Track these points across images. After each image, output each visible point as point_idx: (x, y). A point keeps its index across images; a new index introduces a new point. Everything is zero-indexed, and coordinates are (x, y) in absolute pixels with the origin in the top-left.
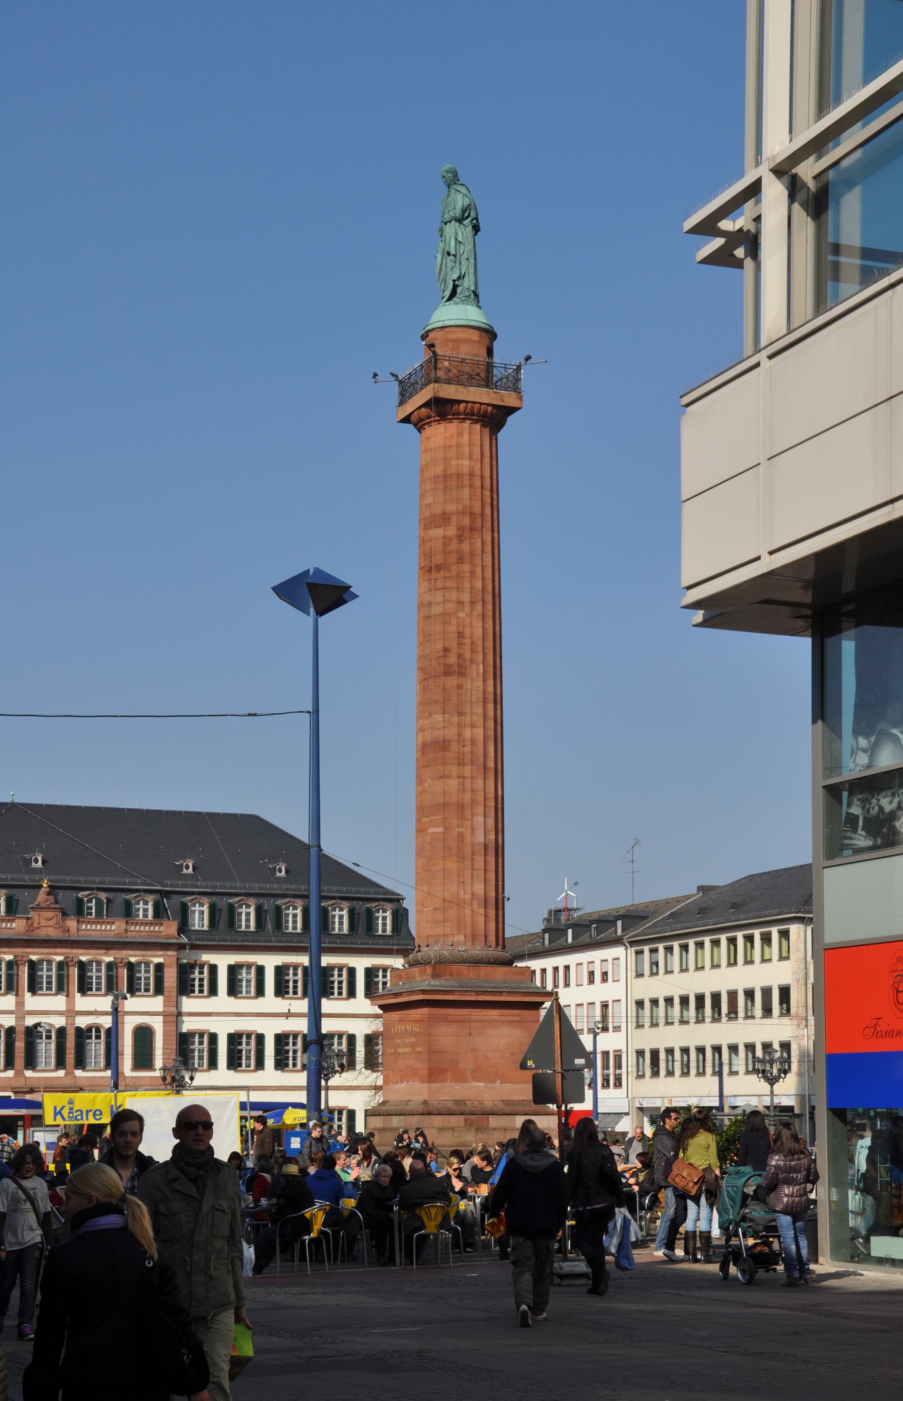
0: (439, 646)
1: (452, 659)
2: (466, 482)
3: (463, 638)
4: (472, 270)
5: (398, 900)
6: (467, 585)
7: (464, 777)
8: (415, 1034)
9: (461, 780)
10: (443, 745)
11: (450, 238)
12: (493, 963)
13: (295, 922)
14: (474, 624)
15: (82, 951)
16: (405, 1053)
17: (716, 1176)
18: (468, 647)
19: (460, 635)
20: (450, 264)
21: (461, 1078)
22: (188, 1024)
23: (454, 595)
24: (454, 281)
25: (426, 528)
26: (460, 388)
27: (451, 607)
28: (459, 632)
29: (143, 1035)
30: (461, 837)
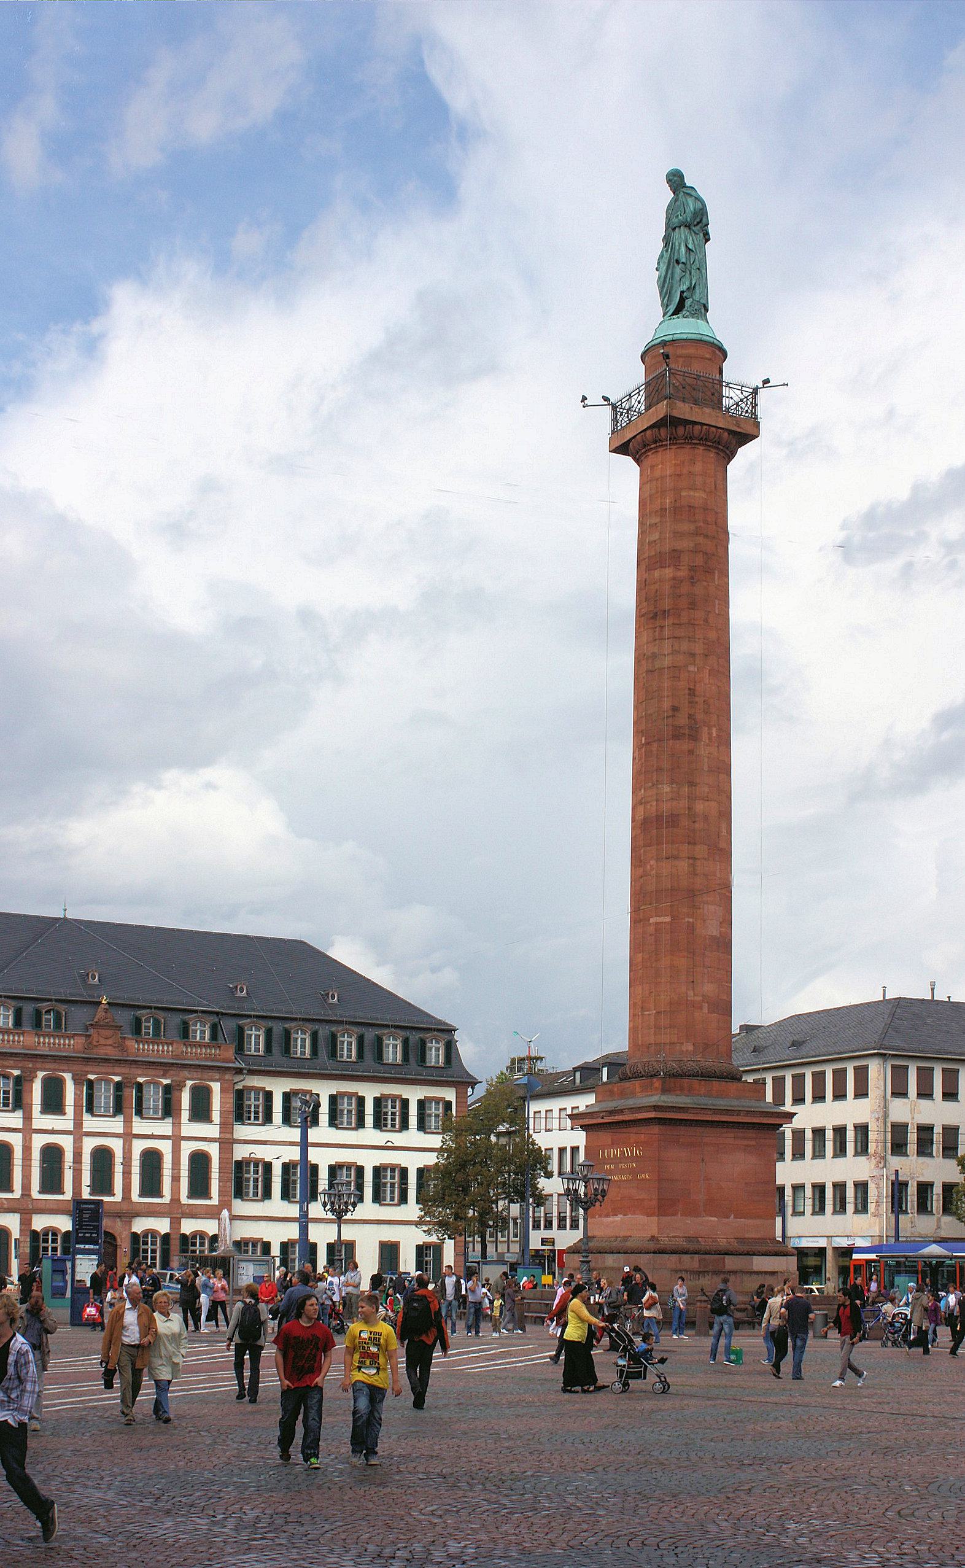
0: (666, 704)
1: (682, 720)
5: (451, 1031)
7: (695, 859)
8: (636, 1159)
9: (691, 861)
10: (673, 820)
11: (680, 245)
12: (726, 1077)
13: (349, 1050)
15: (140, 1072)
16: (621, 1181)
17: (681, 1310)
21: (692, 1211)
22: (241, 1152)
23: (685, 646)
24: (682, 292)
25: (649, 569)
26: (696, 409)
30: (691, 928)
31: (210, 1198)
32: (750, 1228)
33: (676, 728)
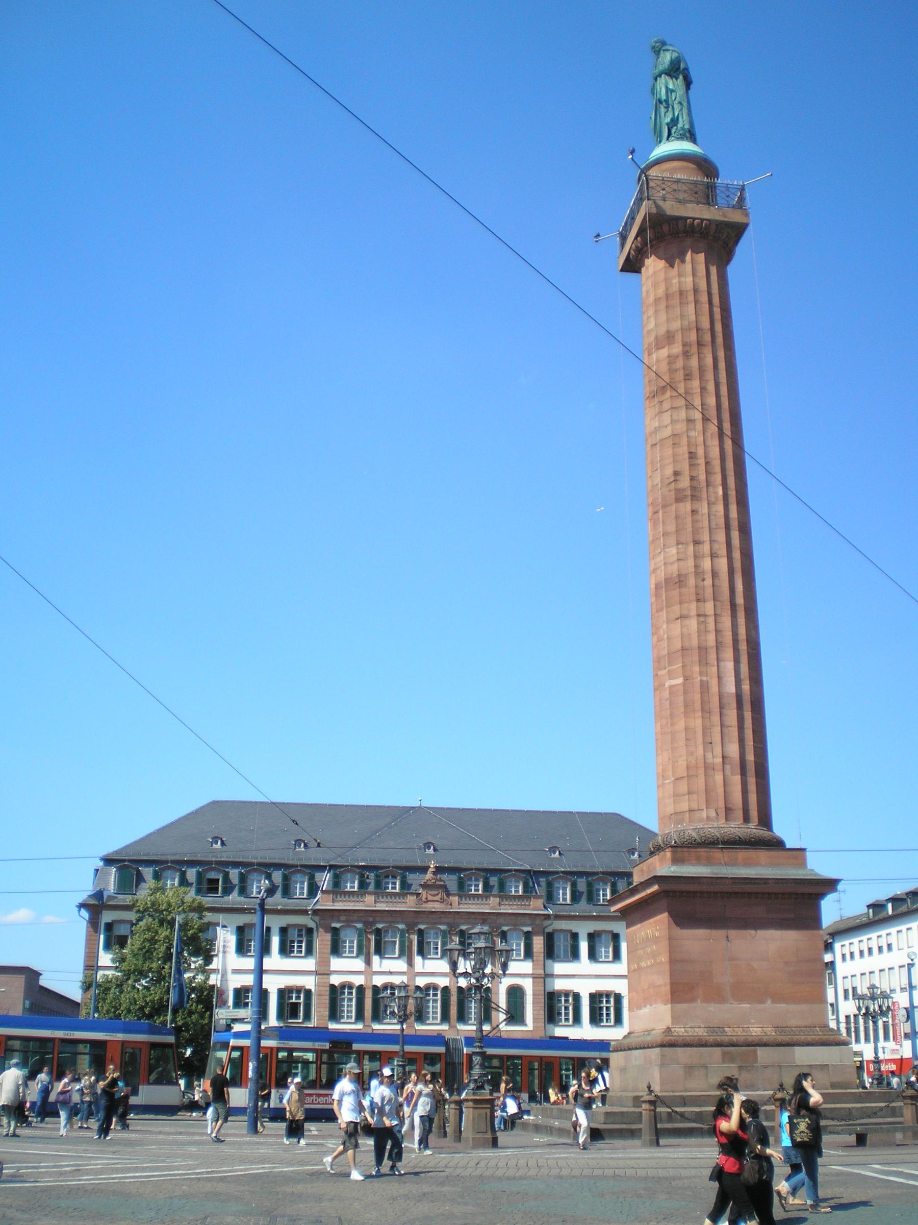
0: (669, 471)
1: (685, 483)
2: (691, 298)
3: (696, 458)
4: (685, 111)
6: (697, 402)
7: (705, 616)
9: (702, 619)
14: (709, 443)
18: (702, 468)
19: (692, 455)
20: (663, 110)
21: (716, 995)
27: (681, 427)
28: (690, 453)
29: (516, 993)
30: (705, 687)
31: (526, 1025)
32: (795, 1015)
33: (677, 491)
